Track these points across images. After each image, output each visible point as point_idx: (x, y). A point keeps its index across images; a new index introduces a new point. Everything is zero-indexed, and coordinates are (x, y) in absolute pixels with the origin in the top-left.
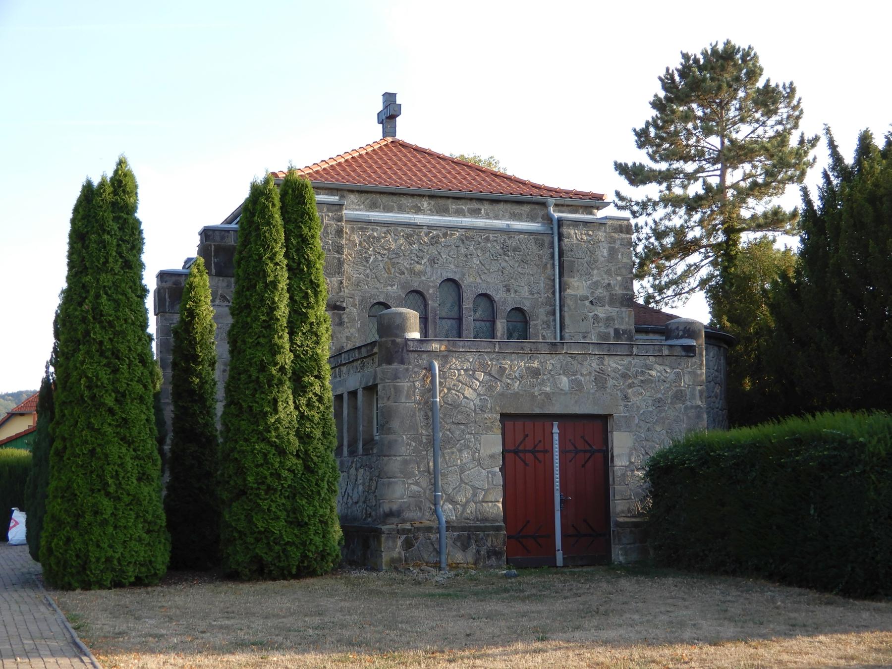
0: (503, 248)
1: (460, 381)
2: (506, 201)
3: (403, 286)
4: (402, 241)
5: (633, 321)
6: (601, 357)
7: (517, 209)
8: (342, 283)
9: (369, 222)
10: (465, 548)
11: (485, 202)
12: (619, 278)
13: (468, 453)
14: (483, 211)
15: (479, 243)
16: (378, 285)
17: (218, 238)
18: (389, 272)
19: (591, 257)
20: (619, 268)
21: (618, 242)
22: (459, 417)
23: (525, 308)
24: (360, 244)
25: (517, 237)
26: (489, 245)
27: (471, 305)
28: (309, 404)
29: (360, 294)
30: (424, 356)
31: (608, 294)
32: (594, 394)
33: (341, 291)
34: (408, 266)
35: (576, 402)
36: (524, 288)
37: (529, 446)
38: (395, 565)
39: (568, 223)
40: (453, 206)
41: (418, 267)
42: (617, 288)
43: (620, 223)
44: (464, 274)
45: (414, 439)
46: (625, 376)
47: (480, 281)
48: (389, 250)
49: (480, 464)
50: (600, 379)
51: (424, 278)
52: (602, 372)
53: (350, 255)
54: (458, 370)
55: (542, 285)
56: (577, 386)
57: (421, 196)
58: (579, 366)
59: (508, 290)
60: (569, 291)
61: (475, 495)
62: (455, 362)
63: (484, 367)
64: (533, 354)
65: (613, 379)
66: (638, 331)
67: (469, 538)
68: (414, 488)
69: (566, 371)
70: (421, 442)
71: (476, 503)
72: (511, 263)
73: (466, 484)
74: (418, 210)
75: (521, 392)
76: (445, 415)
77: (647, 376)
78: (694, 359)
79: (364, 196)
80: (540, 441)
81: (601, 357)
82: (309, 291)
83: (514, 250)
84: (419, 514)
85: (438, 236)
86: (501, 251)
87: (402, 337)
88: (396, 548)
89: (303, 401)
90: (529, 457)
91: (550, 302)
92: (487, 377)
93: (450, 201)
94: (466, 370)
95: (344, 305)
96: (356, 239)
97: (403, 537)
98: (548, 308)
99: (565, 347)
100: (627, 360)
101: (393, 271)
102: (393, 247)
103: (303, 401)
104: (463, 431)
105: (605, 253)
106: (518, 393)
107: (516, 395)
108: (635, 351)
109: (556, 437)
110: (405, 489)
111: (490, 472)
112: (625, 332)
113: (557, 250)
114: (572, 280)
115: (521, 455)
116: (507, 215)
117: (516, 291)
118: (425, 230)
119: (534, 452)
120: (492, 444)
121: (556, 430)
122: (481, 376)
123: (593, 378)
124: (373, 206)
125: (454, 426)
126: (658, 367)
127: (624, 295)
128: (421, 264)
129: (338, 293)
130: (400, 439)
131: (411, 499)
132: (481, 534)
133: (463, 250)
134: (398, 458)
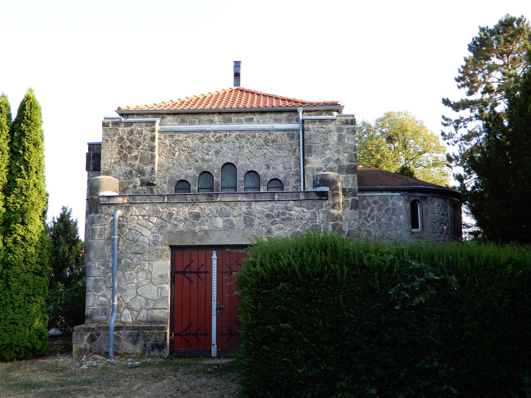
0: (265, 141)
1: (138, 224)
2: (271, 112)
3: (197, 169)
4: (197, 141)
5: (356, 182)
6: (249, 203)
7: (278, 116)
8: (153, 169)
9: (176, 132)
10: (135, 342)
11: (256, 114)
12: (346, 155)
13: (143, 274)
14: (255, 119)
15: (248, 139)
16: (181, 169)
17: (95, 149)
18: (188, 160)
19: (324, 142)
20: (346, 148)
21: (345, 131)
22: (137, 249)
23: (280, 179)
24: (170, 145)
25: (275, 134)
26: (255, 140)
27: (243, 179)
28: (15, 242)
29: (169, 175)
30: (113, 207)
31: (337, 165)
32: (243, 230)
33: (152, 174)
34: (201, 157)
35: (228, 236)
36: (278, 164)
37: (194, 268)
38: (81, 352)
39: (308, 121)
40: (234, 118)
41: (207, 157)
42: (344, 161)
43: (346, 118)
44: (238, 159)
45: (103, 265)
46: (268, 216)
47: (249, 163)
48: (188, 147)
49: (151, 282)
50: (248, 220)
51: (211, 163)
52: (249, 213)
53: (163, 152)
54: (137, 216)
55: (293, 163)
56: (230, 226)
57: (213, 113)
58: (232, 210)
59: (268, 168)
60: (308, 166)
61: (147, 304)
62: (134, 209)
63: (156, 213)
64: (194, 203)
65: (258, 218)
66: (360, 190)
67: (138, 335)
68: (103, 299)
69: (221, 214)
70: (108, 267)
71: (148, 310)
72: (270, 150)
73: (141, 296)
74: (211, 122)
75: (185, 230)
76: (127, 248)
77: (287, 216)
78: (327, 202)
79: (176, 117)
80: (203, 265)
81: (249, 203)
82: (22, 167)
83: (273, 142)
84: (105, 317)
85: (220, 137)
86: (264, 143)
87: (97, 195)
88: (82, 341)
89: (10, 240)
90: (194, 277)
91: (298, 173)
92: (160, 221)
93: (232, 115)
94: (143, 216)
95: (155, 182)
96: (168, 142)
97: (89, 334)
98: (297, 177)
99: (219, 197)
100: (270, 205)
101: (191, 160)
102: (191, 145)
103: (10, 240)
104: (139, 259)
105: (335, 139)
106: (182, 231)
107: (181, 233)
108: (276, 197)
109: (215, 262)
110: (95, 300)
111: (160, 287)
112: (350, 190)
113: (301, 139)
114: (310, 158)
115: (188, 275)
116: (272, 120)
117: (274, 168)
118: (213, 133)
119: (197, 272)
120: (163, 266)
121: (214, 256)
122: (155, 220)
123: (242, 218)
124: (183, 122)
125: (133, 256)
126: (296, 208)
127: (349, 165)
128: (209, 155)
129: (151, 175)
130: (93, 265)
131: (99, 307)
132: (148, 332)
133: (237, 144)
134: (92, 278)
